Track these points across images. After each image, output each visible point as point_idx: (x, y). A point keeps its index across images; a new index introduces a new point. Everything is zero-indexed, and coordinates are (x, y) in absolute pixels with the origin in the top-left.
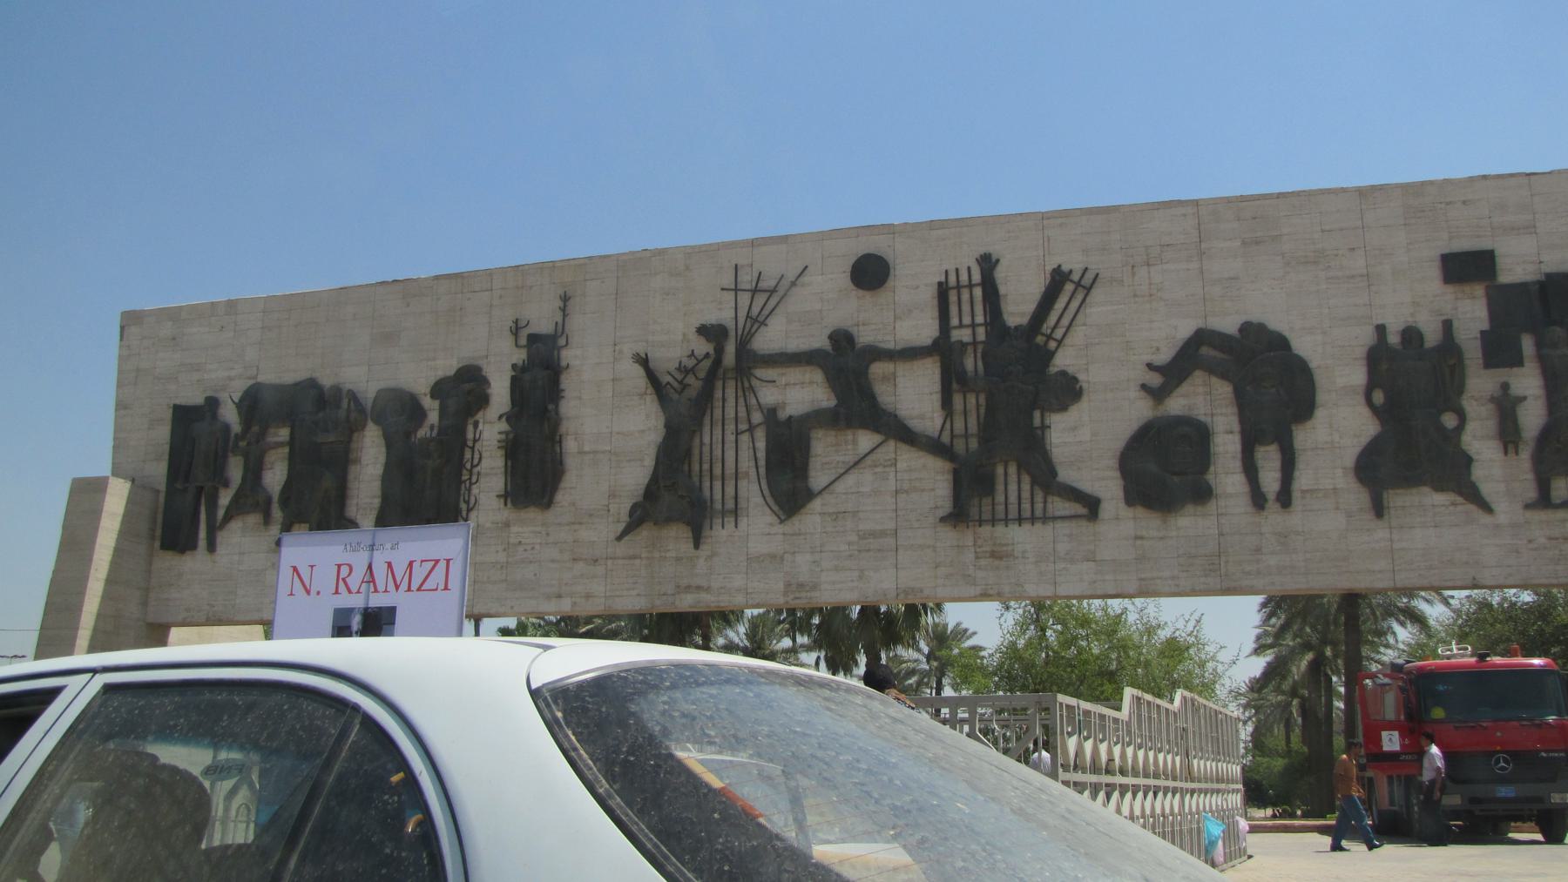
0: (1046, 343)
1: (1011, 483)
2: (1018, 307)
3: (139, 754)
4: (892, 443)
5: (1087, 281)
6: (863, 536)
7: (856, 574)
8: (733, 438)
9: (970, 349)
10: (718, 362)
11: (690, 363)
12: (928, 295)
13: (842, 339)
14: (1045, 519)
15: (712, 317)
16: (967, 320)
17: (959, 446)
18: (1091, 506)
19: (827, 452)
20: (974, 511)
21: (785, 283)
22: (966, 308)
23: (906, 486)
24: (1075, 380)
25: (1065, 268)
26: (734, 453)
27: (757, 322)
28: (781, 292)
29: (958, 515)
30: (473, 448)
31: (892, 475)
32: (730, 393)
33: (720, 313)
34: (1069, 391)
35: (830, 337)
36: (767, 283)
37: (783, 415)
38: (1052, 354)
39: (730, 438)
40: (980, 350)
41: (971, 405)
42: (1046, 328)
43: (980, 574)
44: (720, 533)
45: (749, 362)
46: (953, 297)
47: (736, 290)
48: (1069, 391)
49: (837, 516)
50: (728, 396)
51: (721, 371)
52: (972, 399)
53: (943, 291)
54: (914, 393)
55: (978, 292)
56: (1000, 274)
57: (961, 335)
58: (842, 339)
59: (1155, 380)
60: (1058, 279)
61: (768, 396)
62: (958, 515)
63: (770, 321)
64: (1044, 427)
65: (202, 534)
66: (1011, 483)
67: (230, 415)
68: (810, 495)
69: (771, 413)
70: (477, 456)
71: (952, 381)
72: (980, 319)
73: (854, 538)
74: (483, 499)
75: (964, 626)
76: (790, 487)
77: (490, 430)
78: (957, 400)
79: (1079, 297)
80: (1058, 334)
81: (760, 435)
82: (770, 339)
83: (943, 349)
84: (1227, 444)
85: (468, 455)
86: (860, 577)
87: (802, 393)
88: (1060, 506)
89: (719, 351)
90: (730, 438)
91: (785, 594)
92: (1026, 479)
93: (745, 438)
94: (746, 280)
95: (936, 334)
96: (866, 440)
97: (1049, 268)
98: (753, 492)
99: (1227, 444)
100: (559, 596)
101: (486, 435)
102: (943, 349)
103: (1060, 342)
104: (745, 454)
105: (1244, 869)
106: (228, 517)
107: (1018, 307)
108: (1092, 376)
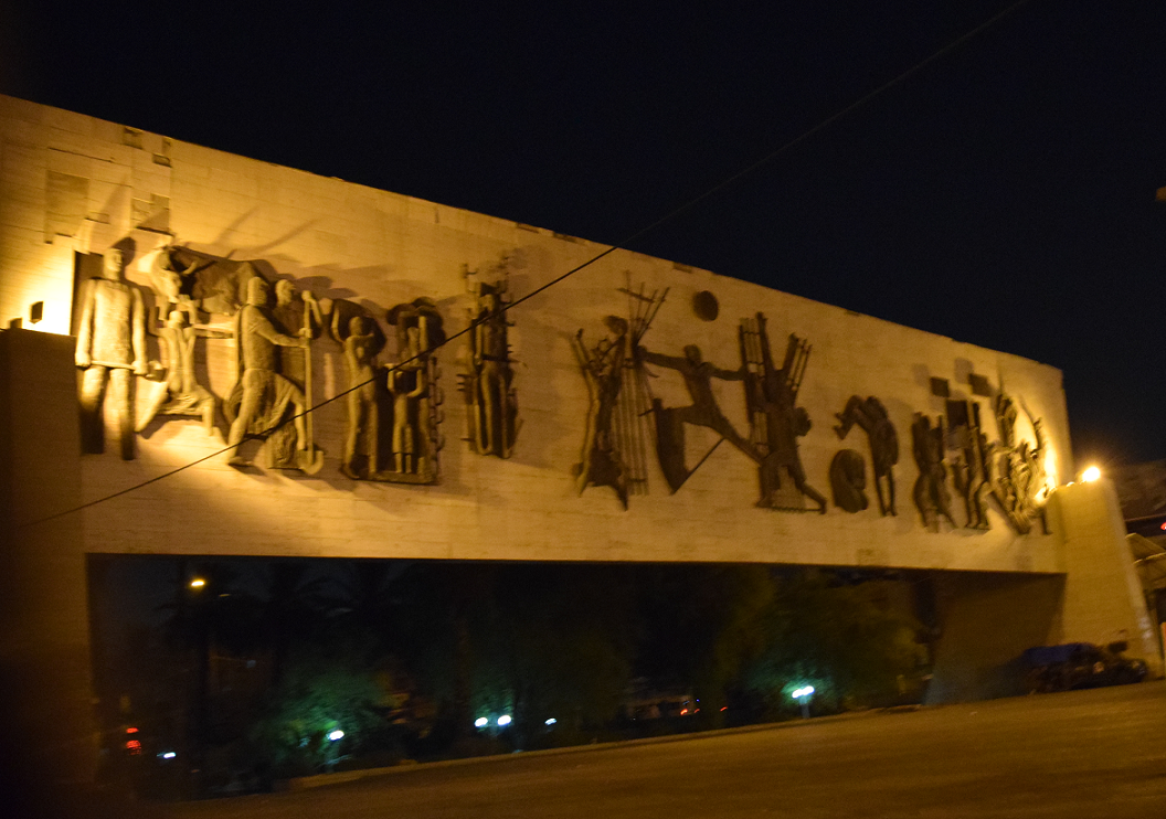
0: (791, 386)
3: (386, 282)
5: (806, 348)
11: (604, 347)
12: (734, 334)
21: (659, 295)
32: (633, 381)
33: (621, 309)
45: (640, 356)
54: (731, 399)
57: (753, 368)
59: (838, 423)
68: (687, 474)
77: (458, 354)
78: (757, 415)
79: (804, 358)
87: (672, 390)
100: (528, 545)
101: (445, 374)
104: (645, 426)
105: (825, 519)
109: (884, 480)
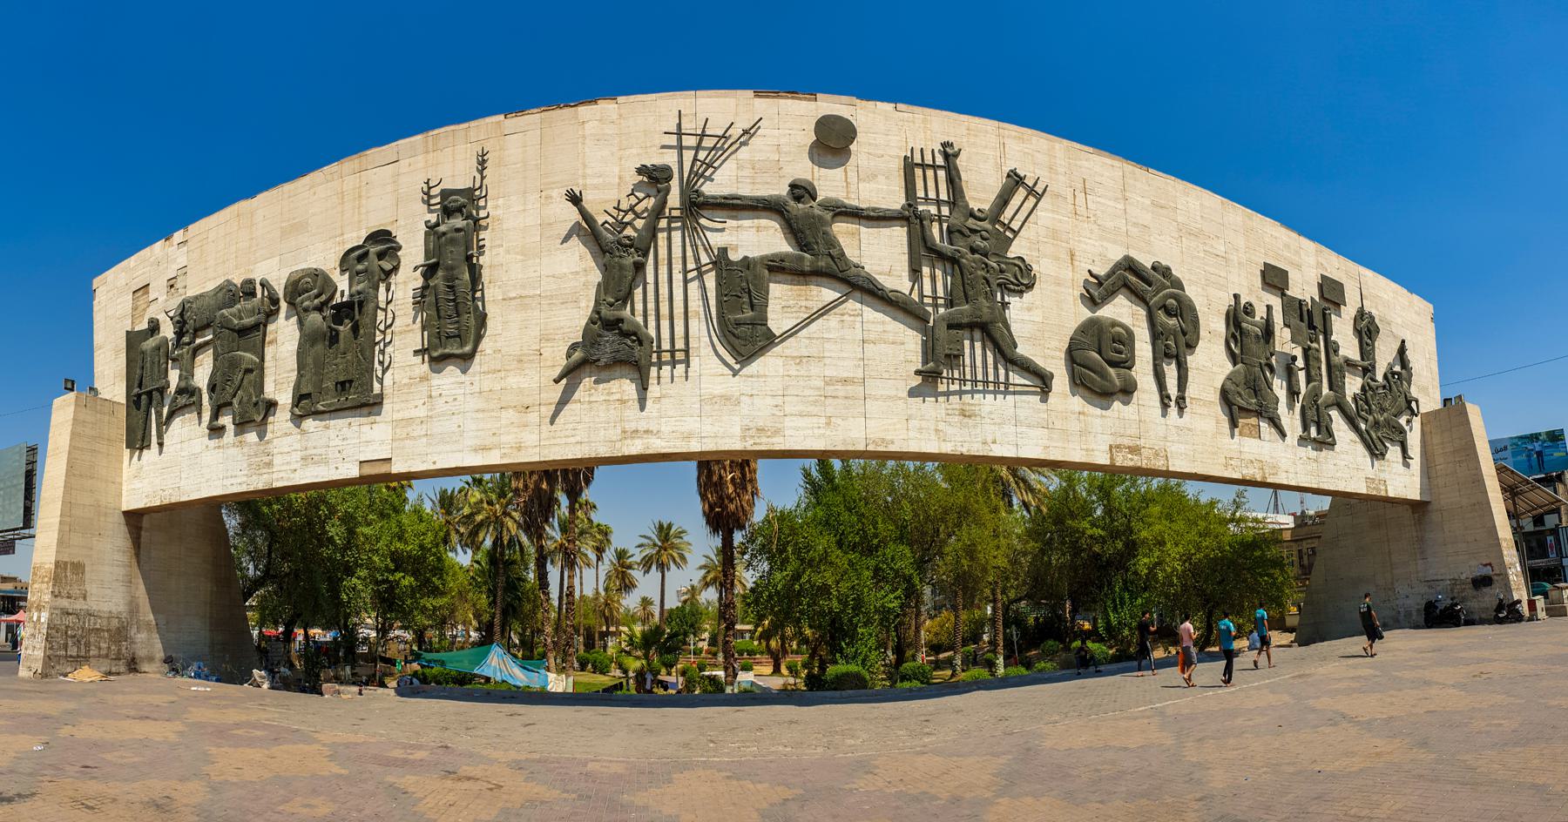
6: (829, 381)
7: (823, 420)
8: (681, 276)
9: (936, 225)
13: (801, 191)
16: (932, 195)
18: (1043, 382)
21: (735, 132)
22: (931, 184)
23: (872, 336)
26: (678, 300)
30: (385, 310)
31: (858, 325)
34: (1021, 279)
35: (793, 186)
36: (716, 129)
39: (678, 277)
43: (950, 431)
44: (663, 382)
46: (918, 172)
48: (1021, 279)
49: (800, 360)
50: (672, 243)
53: (909, 167)
54: (881, 254)
55: (942, 174)
56: (961, 162)
60: (1015, 180)
64: (1005, 305)
65: (154, 439)
66: (975, 353)
67: (168, 331)
68: (770, 340)
69: (721, 260)
70: (390, 315)
71: (922, 251)
72: (944, 196)
73: (820, 383)
74: (397, 358)
76: (745, 336)
79: (1032, 200)
81: (710, 281)
82: (719, 184)
84: (1143, 349)
85: (380, 316)
86: (828, 424)
87: (759, 239)
88: (1015, 378)
90: (678, 277)
91: (744, 438)
93: (694, 287)
96: (826, 294)
97: (1006, 170)
98: (701, 332)
99: (1143, 349)
102: (909, 217)
103: (1016, 233)
104: (695, 303)
106: (171, 415)
107: (980, 197)
108: (1042, 267)
109: (1171, 371)
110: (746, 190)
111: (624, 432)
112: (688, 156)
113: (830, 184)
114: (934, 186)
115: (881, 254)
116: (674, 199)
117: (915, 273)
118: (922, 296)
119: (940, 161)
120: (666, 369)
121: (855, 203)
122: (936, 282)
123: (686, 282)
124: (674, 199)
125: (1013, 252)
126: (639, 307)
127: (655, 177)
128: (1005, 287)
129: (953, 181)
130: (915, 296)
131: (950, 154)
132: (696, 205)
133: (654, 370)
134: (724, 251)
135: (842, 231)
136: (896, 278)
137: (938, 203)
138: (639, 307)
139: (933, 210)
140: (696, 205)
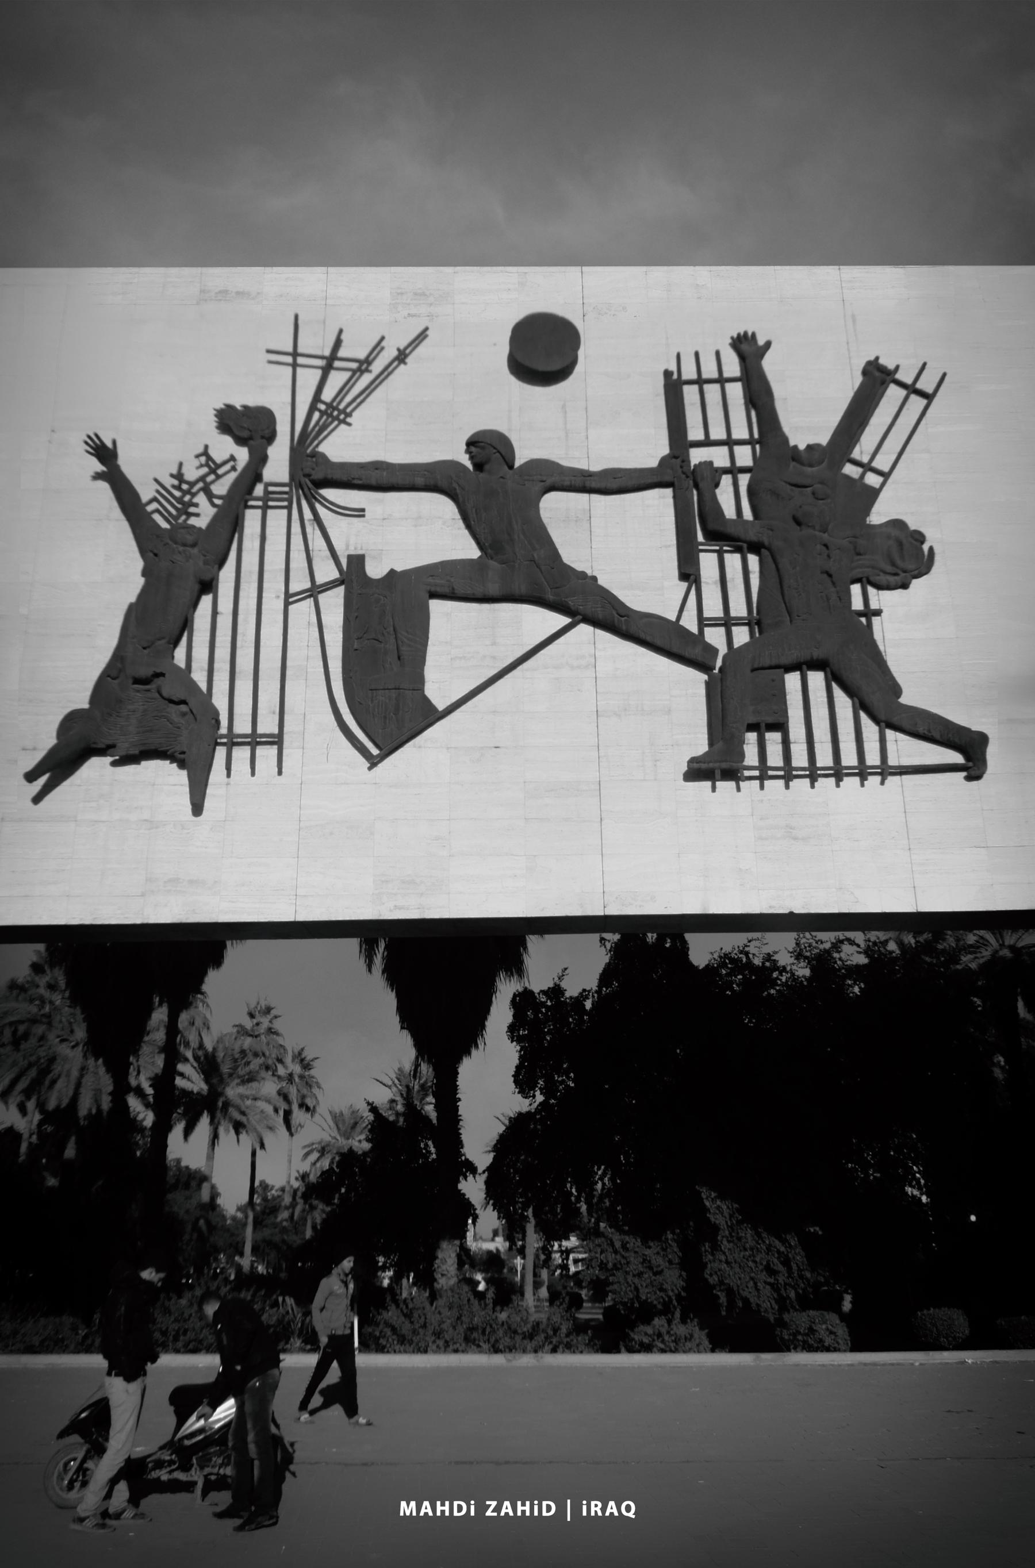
1: (810, 698)
2: (808, 424)
4: (584, 630)
9: (726, 480)
10: (253, 473)
13: (489, 449)
14: (885, 771)
15: (244, 397)
17: (715, 637)
19: (460, 640)
20: (751, 757)
24: (919, 538)
25: (888, 362)
26: (271, 640)
27: (332, 414)
28: (377, 367)
29: (717, 767)
33: (272, 392)
35: (472, 444)
36: (354, 349)
37: (375, 570)
38: (874, 493)
39: (273, 604)
40: (744, 480)
41: (732, 581)
42: (862, 450)
44: (232, 781)
46: (690, 394)
47: (295, 354)
50: (269, 537)
51: (259, 490)
52: (733, 561)
53: (673, 388)
54: (626, 546)
55: (736, 392)
56: (769, 364)
58: (489, 449)
60: (877, 378)
61: (348, 537)
62: (717, 767)
63: (354, 414)
66: (810, 698)
68: (430, 715)
71: (701, 529)
72: (740, 432)
75: (735, 336)
76: (387, 698)
78: (708, 562)
80: (883, 462)
81: (334, 603)
83: (678, 475)
87: (425, 533)
88: (905, 749)
89: (259, 460)
90: (273, 604)
92: (844, 703)
94: (316, 342)
95: (665, 450)
102: (678, 475)
103: (886, 476)
107: (808, 424)
110: (399, 455)
111: (202, 291)
112: (309, 379)
113: (540, 425)
114: (722, 420)
115: (626, 546)
116: (278, 467)
117: (689, 573)
118: (703, 622)
119: (732, 366)
120: (241, 754)
121: (582, 465)
122: (732, 581)
123: (289, 599)
124: (278, 467)
125: (879, 515)
126: (200, 653)
127: (247, 425)
128: (537, 1006)
129: (759, 396)
130: (689, 622)
131: (749, 350)
132: (314, 476)
133: (221, 753)
134: (357, 561)
135: (555, 508)
136: (649, 583)
137: (730, 443)
138: (200, 653)
139: (719, 457)
140: (314, 476)
